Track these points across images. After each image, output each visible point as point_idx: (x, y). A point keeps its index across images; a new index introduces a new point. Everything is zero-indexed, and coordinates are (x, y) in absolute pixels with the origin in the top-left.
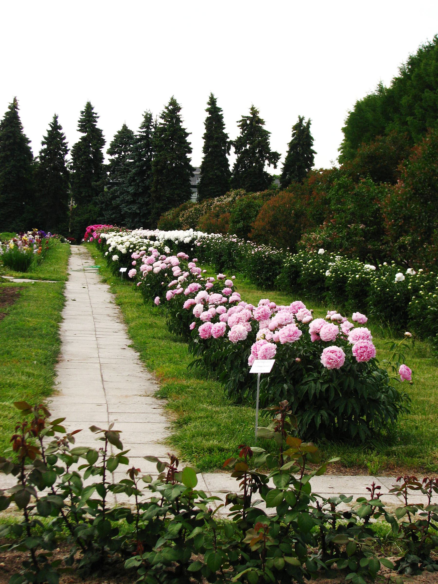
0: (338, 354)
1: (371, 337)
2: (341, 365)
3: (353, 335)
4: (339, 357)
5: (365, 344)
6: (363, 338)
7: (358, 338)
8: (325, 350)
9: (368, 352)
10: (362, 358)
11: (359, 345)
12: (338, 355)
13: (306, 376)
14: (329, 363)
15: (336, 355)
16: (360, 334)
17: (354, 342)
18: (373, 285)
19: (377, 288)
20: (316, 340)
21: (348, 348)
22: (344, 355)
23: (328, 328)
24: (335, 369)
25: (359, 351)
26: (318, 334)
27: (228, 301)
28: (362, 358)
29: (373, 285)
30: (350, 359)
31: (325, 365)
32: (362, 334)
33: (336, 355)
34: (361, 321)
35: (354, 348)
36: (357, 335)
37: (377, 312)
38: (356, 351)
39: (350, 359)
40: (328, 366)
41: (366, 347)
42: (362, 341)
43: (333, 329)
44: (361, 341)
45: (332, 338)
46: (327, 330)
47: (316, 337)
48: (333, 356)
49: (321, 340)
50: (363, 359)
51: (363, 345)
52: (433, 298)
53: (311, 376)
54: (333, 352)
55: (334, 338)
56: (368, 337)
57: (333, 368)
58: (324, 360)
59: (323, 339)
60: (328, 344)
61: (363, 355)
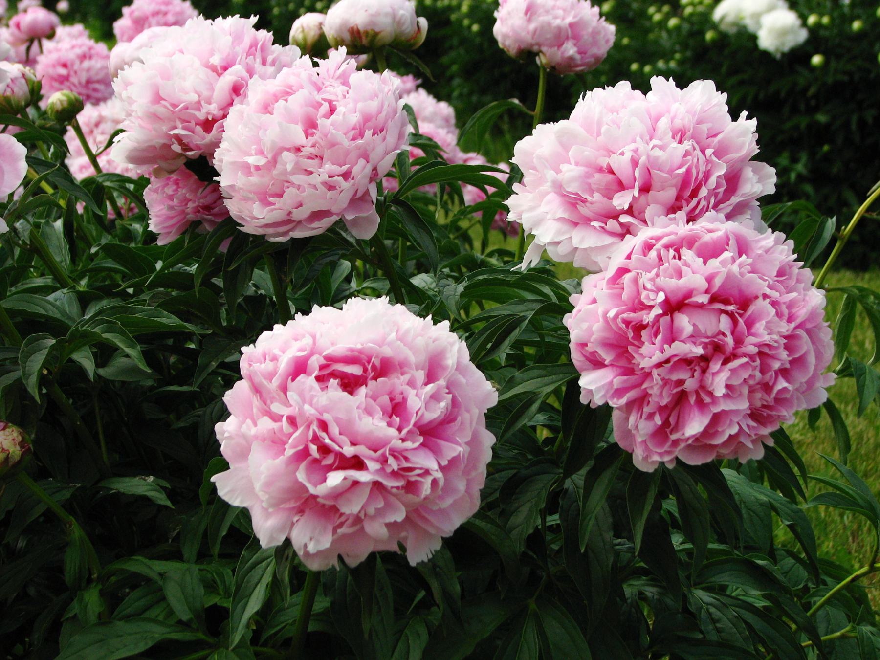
0: (415, 402)
1: (762, 181)
2: (459, 506)
3: (570, 172)
4: (431, 433)
5: (724, 266)
6: (686, 197)
7: (615, 198)
8: (271, 351)
9: (764, 354)
10: (695, 426)
11: (655, 285)
12: (419, 402)
13: (92, 600)
14: (306, 504)
15: (396, 409)
16: (647, 151)
17: (585, 239)
18: (459, 22)
19: (469, 27)
20: (191, 228)
21: (513, 313)
22: (484, 391)
23: (296, 103)
24: (392, 561)
25: (649, 354)
26: (202, 169)
27: (861, 302)
28: (695, 426)
29: (459, 22)
30: (550, 440)
31: (266, 528)
32: (672, 154)
33: (396, 409)
34: (570, 50)
35: (588, 317)
36: (621, 163)
37: (470, 94)
38: (623, 343)
39: (550, 440)
40: (312, 541)
41: (732, 300)
42: (679, 227)
43: (348, 114)
44: (663, 227)
45: (338, 202)
46: (282, 127)
47: (190, 197)
48: (359, 416)
49: (229, 224)
50: (700, 442)
51: (695, 275)
52: (669, 32)
53: (134, 600)
54: (351, 373)
55: (358, 200)
56: (732, 180)
57: (358, 555)
58: (253, 471)
59: (253, 215)
60: (310, 267)
61: (702, 398)
